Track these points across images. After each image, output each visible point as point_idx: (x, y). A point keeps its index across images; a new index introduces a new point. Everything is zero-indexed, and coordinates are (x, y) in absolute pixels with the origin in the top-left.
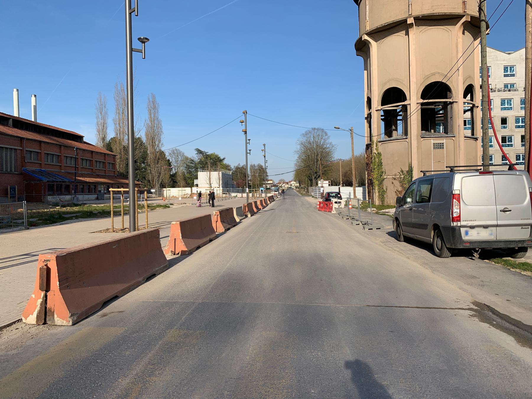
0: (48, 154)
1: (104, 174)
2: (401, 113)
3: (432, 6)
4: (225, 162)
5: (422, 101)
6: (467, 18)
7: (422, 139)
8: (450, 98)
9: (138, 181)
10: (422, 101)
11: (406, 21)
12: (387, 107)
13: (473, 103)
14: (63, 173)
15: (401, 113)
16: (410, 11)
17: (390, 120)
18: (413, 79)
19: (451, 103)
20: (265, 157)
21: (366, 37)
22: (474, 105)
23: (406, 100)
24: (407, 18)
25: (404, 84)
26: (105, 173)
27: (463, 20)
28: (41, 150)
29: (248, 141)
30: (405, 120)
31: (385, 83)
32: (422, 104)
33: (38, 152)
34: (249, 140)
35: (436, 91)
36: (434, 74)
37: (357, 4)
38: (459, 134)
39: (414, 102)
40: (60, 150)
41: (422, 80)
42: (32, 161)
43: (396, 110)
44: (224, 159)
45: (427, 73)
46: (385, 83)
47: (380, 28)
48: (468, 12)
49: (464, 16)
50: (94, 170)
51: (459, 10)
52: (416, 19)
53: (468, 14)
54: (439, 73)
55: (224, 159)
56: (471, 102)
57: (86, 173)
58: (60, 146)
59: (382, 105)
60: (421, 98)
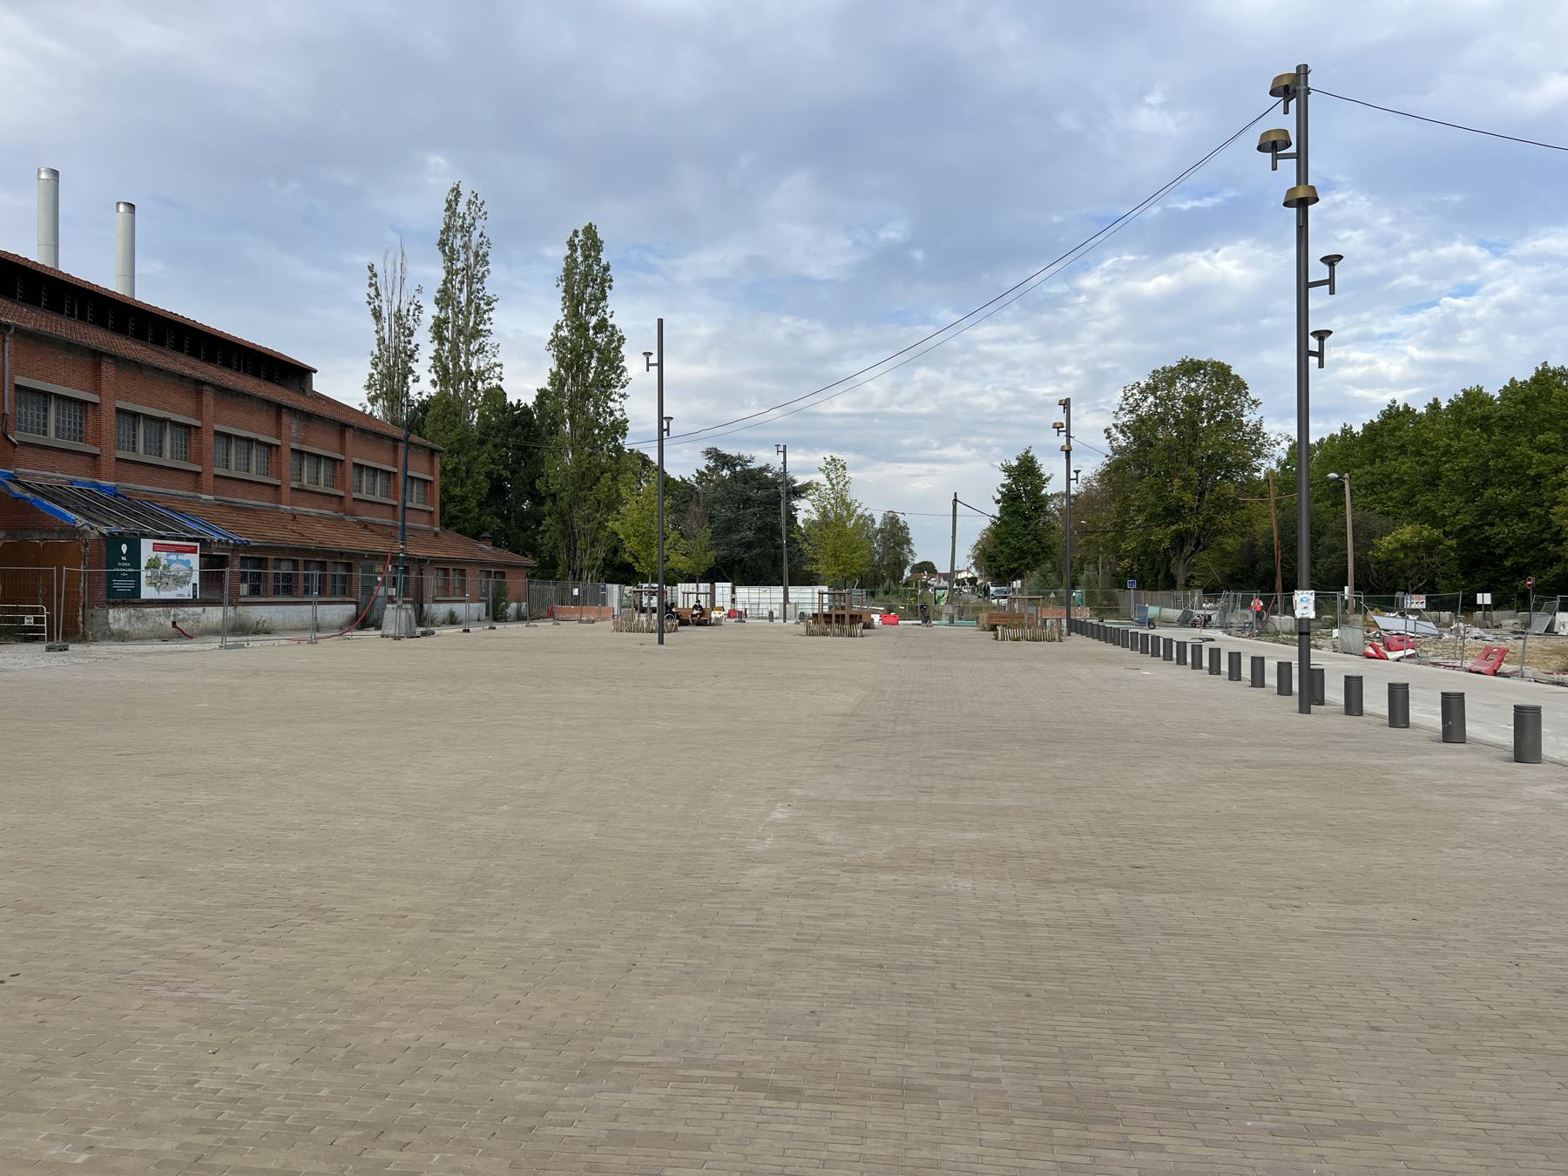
0: (229, 436)
1: (389, 522)
14: (205, 504)
28: (279, 438)
40: (199, 403)
42: (322, 488)
50: (348, 502)
57: (313, 511)
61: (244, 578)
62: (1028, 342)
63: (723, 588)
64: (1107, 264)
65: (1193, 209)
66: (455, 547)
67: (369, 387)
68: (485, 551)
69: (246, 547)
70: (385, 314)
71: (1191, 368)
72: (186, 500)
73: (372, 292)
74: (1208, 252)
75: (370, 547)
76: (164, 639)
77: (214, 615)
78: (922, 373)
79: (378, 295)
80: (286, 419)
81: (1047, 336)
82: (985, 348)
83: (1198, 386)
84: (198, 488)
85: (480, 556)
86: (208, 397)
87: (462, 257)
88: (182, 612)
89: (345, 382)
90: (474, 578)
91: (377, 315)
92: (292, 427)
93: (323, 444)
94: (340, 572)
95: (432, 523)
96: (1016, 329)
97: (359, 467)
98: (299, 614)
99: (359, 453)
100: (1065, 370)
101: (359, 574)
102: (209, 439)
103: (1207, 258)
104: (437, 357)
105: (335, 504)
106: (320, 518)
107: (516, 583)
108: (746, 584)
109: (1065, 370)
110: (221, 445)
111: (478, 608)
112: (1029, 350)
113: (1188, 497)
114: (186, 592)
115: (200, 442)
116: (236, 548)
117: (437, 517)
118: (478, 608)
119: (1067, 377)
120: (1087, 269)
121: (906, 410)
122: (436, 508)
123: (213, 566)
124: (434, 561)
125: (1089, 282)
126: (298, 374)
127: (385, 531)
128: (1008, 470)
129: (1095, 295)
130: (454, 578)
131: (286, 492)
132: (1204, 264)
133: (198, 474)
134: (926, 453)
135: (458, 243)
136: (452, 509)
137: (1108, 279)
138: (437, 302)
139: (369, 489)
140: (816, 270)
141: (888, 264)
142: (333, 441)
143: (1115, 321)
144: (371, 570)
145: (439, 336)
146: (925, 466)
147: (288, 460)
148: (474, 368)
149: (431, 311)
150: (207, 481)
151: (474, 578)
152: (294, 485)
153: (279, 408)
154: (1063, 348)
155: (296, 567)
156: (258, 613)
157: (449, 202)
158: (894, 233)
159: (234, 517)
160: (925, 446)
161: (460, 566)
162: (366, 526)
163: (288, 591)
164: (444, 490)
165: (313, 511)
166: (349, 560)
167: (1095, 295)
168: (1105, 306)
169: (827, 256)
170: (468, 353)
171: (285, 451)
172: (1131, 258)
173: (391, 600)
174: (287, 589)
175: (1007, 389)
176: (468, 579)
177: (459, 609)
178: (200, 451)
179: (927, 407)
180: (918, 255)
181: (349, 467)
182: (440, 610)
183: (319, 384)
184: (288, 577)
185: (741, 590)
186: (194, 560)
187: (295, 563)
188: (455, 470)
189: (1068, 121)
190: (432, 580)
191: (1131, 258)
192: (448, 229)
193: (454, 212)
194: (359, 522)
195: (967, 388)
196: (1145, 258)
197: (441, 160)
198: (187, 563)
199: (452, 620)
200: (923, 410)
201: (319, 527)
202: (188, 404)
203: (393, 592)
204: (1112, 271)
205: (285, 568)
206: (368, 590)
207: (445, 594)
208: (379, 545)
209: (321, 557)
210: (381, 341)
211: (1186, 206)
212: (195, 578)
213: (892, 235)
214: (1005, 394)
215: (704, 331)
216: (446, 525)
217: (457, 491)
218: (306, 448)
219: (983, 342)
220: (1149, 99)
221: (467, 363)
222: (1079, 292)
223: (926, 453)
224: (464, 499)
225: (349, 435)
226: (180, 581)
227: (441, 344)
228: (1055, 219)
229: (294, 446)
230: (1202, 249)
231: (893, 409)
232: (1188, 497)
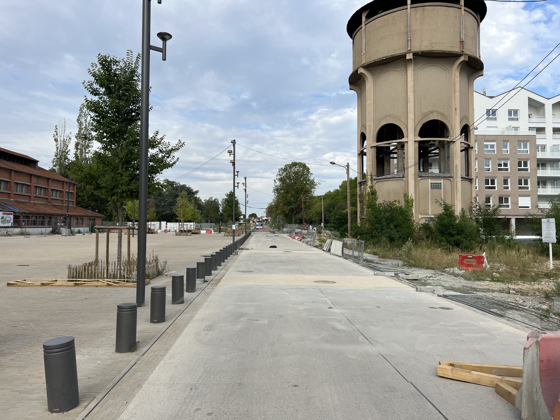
0: (17, 183)
1: (61, 205)
2: (395, 151)
3: (431, 44)
4: (198, 196)
5: (420, 139)
6: (464, 57)
7: (420, 179)
8: (447, 137)
9: (238, 236)
10: (420, 139)
11: (404, 56)
12: (381, 144)
13: (469, 143)
14: (12, 201)
15: (395, 151)
16: (409, 47)
17: (382, 158)
18: (411, 116)
19: (449, 143)
20: (245, 191)
21: (361, 71)
22: (469, 145)
23: (403, 137)
24: (406, 53)
25: (402, 121)
26: (63, 203)
27: (462, 59)
28: (31, 183)
29: (236, 174)
30: (402, 158)
31: (382, 119)
32: (420, 143)
33: (7, 181)
34: (238, 172)
35: (434, 129)
36: (432, 112)
37: (351, 37)
38: (456, 174)
39: (411, 140)
40: (10, 175)
41: (420, 118)
42: (42, 196)
43: (389, 147)
44: (197, 192)
45: (425, 111)
46: (382, 119)
47: (378, 62)
48: (466, 52)
49: (462, 55)
50: (49, 199)
51: (456, 49)
52: (415, 54)
53: (466, 54)
54: (436, 111)
55: (197, 192)
56: (466, 142)
57: (40, 202)
58: (11, 170)
59: (377, 142)
60: (419, 136)
61: (23, 221)
62: (292, 137)
63: (163, 223)
64: (319, 111)
65: (347, 94)
66: (80, 212)
67: (53, 162)
68: (89, 212)
69: (25, 213)
70: (59, 140)
71: (295, 164)
72: (7, 201)
73: (55, 134)
74: (351, 109)
75: (56, 212)
76: (4, 236)
77: (17, 230)
78: (256, 146)
79: (57, 134)
80: (33, 178)
81: (299, 135)
82: (277, 138)
83: (296, 169)
84: (10, 197)
85: (88, 214)
86: (13, 173)
87: (84, 124)
88: (9, 229)
89: (46, 162)
90: (86, 221)
91: (56, 140)
92: (34, 180)
93: (43, 184)
94: (48, 219)
95: (73, 204)
96: (288, 132)
97: (53, 190)
98: (39, 230)
99: (53, 186)
100: (305, 147)
101: (53, 220)
102: (13, 184)
103: (352, 111)
104: (76, 154)
105: (45, 200)
106: (42, 204)
107: (98, 221)
108: (171, 222)
109: (305, 147)
110: (16, 186)
111: (87, 229)
112: (293, 140)
113: (292, 199)
114: (10, 225)
115: (10, 185)
116: (22, 213)
117: (75, 203)
118: (87, 229)
119: (305, 150)
120: (312, 113)
121: (251, 159)
122: (75, 200)
123: (16, 218)
124: (74, 216)
125: (313, 117)
126: (35, 162)
127: (61, 208)
128: (227, 195)
129: (315, 122)
130: (80, 221)
131: (32, 197)
132: (351, 113)
133: (9, 194)
134: (258, 175)
135: (83, 120)
136: (80, 200)
137: (319, 116)
138: (76, 137)
139: (55, 196)
140: (218, 107)
141: (244, 106)
142: (46, 183)
143: (321, 131)
144: (56, 219)
145: (77, 148)
146: (258, 179)
147: (33, 189)
148: (87, 157)
149: (74, 140)
150: (12, 196)
151: (86, 221)
152: (35, 195)
153: (31, 175)
154: (304, 140)
155: (37, 218)
156: (28, 230)
157: (81, 108)
158: (245, 96)
159: (20, 205)
160: (258, 172)
161: (82, 217)
162: (54, 206)
163: (34, 224)
164: (77, 194)
165: (40, 202)
166: (51, 216)
167: (315, 122)
168: (318, 125)
169: (223, 103)
170: (85, 152)
171: (33, 187)
172: (326, 110)
173: (62, 227)
174: (34, 224)
175: (286, 153)
176: (84, 221)
177: (82, 229)
178: (10, 188)
179: (258, 158)
180: (254, 104)
181: (50, 190)
182: (76, 229)
183: (39, 165)
184: (35, 221)
185: (168, 224)
186: (12, 216)
187: (36, 217)
188: (80, 188)
189: (305, 61)
190: (74, 221)
191: (326, 110)
192: (80, 116)
193: (82, 112)
194: (53, 205)
195: (271, 152)
196: (331, 110)
197: (71, 57)
198: (10, 217)
199: (79, 232)
200: (257, 159)
201: (42, 207)
202: (8, 176)
203: (63, 224)
204: (320, 114)
205: (34, 218)
206: (56, 224)
207: (78, 225)
208: (60, 212)
209: (43, 216)
210: (57, 148)
211: (344, 93)
212: (12, 221)
213: (245, 97)
214: (285, 155)
215: (176, 127)
216: (77, 205)
217: (81, 194)
218: (38, 185)
219: (278, 136)
220: (332, 55)
221: (85, 156)
222: (310, 121)
223: (258, 175)
224: (83, 196)
225: (50, 181)
226: (8, 222)
227: (77, 150)
228: (301, 95)
229: (35, 185)
230: (349, 108)
231: (246, 158)
232: (292, 199)
